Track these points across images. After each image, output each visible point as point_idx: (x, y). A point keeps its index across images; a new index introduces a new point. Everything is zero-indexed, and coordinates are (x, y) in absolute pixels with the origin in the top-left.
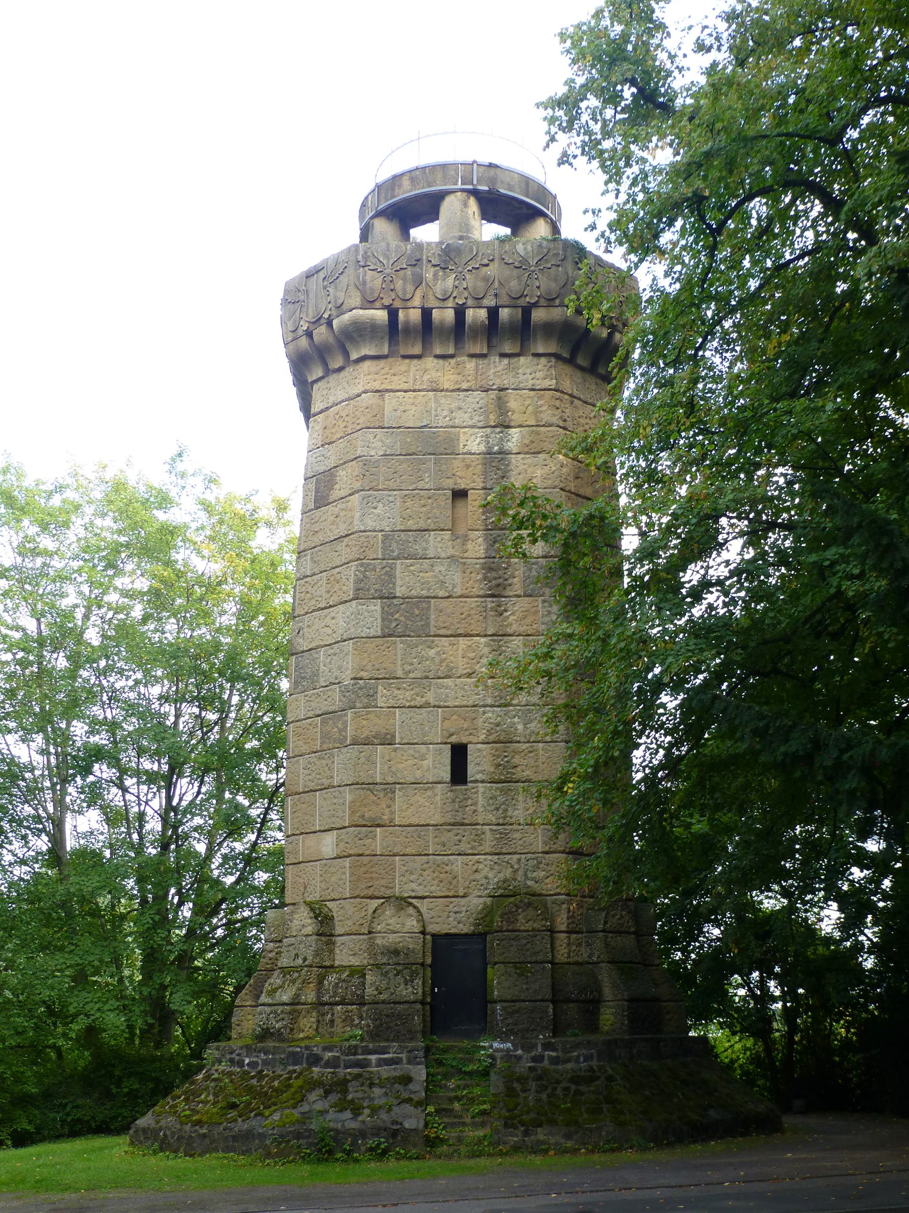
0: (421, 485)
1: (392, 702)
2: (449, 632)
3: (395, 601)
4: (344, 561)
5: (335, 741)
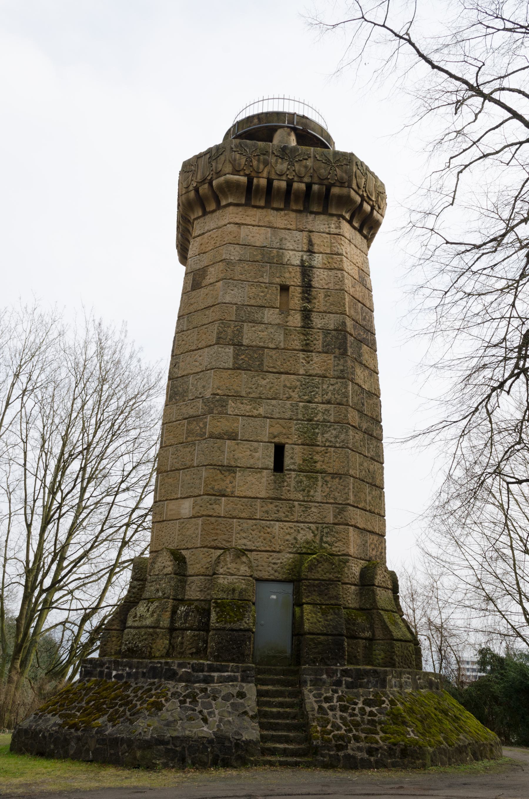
0: (261, 280)
1: (237, 412)
2: (275, 370)
3: (242, 348)
4: (210, 321)
5: (197, 436)
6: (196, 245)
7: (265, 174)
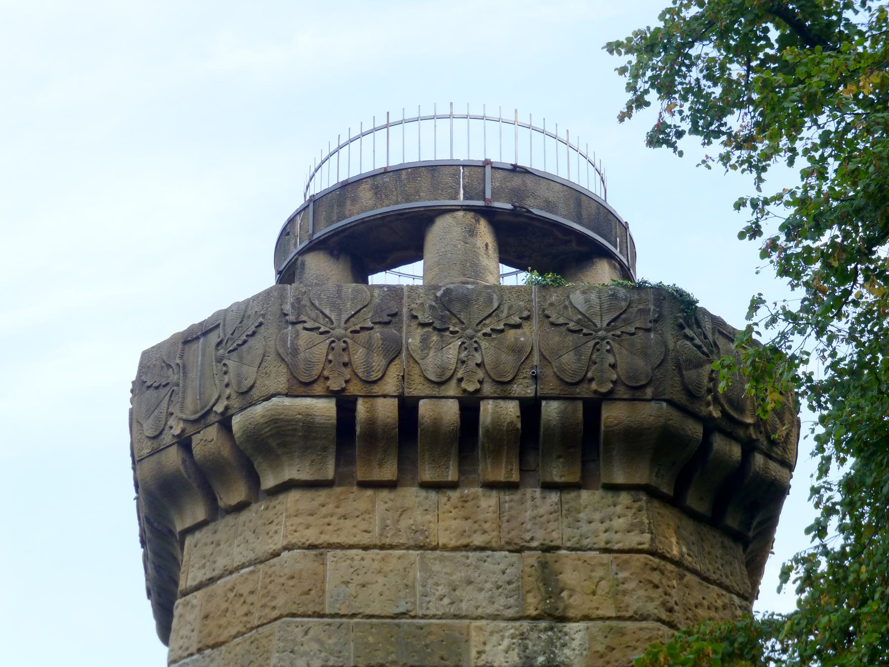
6: (190, 617)
7: (391, 385)
